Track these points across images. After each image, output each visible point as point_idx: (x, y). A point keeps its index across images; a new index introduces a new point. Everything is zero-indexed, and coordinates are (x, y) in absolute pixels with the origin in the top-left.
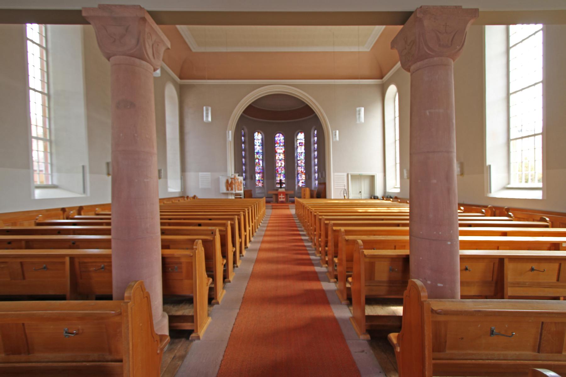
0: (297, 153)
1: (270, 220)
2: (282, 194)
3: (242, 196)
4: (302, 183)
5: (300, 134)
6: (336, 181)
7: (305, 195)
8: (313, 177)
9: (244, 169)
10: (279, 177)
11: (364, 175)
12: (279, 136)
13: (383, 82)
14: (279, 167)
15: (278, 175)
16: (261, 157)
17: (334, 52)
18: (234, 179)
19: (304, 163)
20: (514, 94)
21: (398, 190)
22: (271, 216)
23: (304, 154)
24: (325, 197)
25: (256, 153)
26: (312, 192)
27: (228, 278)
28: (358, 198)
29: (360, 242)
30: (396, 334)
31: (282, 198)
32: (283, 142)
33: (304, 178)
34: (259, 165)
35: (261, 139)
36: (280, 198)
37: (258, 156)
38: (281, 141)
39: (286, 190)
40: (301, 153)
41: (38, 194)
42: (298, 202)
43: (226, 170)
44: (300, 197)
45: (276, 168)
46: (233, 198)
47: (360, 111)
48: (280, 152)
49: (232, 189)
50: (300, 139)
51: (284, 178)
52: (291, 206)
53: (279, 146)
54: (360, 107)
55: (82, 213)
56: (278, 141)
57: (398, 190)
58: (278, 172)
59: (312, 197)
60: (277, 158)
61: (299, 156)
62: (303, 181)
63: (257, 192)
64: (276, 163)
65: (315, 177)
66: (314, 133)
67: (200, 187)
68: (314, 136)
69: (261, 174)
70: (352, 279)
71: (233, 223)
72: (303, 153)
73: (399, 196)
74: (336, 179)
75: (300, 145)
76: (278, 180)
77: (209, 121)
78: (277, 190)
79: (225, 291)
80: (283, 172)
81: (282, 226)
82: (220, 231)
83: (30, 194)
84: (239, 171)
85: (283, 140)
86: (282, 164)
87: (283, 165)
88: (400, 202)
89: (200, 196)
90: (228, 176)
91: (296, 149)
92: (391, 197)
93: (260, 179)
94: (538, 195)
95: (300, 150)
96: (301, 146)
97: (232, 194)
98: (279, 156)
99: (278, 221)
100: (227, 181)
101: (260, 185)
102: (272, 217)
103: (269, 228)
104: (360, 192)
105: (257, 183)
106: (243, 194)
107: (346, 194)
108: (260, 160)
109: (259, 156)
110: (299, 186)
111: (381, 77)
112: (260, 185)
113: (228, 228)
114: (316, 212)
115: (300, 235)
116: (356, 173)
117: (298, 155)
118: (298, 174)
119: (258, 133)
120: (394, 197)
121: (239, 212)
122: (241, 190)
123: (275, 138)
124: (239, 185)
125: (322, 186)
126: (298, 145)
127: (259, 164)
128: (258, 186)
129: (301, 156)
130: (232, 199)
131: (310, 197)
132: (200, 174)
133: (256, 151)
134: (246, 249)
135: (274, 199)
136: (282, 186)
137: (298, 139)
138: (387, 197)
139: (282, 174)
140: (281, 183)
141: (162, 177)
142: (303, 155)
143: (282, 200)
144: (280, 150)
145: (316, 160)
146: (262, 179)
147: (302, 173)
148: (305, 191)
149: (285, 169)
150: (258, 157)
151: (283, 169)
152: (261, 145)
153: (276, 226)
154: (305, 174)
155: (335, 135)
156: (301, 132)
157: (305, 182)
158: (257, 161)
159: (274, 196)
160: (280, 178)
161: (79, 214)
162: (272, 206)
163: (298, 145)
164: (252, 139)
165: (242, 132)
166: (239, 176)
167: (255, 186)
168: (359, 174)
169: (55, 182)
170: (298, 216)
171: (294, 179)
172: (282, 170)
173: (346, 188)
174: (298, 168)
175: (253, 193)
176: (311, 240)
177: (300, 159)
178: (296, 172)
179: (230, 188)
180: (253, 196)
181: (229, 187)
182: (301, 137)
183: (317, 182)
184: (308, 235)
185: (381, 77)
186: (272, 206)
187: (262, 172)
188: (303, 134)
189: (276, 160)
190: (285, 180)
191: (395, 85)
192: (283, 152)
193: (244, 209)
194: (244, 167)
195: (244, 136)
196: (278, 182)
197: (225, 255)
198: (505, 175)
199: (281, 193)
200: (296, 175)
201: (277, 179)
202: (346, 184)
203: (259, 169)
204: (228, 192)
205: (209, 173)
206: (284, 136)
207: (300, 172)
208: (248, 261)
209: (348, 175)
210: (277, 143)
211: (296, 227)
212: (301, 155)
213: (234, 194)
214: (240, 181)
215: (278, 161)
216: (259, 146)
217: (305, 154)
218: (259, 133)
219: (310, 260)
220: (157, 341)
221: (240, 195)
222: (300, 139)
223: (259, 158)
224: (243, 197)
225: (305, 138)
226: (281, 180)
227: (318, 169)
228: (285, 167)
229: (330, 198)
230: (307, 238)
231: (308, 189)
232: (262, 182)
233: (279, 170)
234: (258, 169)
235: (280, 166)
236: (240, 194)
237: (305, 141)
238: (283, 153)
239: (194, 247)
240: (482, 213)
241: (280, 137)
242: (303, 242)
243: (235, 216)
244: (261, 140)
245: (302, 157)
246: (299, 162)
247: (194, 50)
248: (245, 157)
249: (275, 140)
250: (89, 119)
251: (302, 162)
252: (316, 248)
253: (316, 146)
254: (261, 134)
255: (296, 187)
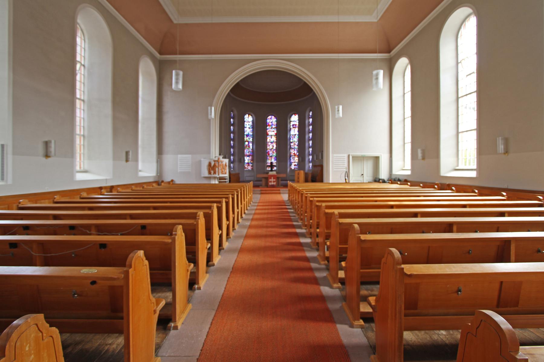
0: (290, 135)
1: (256, 209)
2: (272, 178)
3: (228, 180)
4: (295, 165)
5: (293, 116)
6: (335, 163)
7: (298, 178)
8: (307, 159)
9: (232, 152)
10: (270, 160)
11: (368, 156)
12: (271, 118)
13: (390, 56)
14: (270, 149)
15: (268, 157)
16: (251, 140)
17: (338, 23)
18: (218, 161)
19: (297, 146)
20: (462, 98)
21: (409, 173)
22: (259, 203)
23: (298, 137)
24: (321, 181)
25: (245, 136)
26: (306, 175)
27: (212, 261)
28: (360, 182)
29: (356, 226)
30: (345, 262)
31: (272, 182)
32: (275, 124)
33: (297, 161)
34: (249, 148)
35: (252, 122)
36: (271, 182)
37: (247, 138)
38: (273, 123)
39: (277, 173)
40: (294, 136)
41: (80, 177)
42: (292, 187)
43: (209, 152)
44: (293, 181)
45: (267, 151)
46: (217, 182)
47: (377, 75)
48: (272, 134)
49: (215, 173)
50: (293, 121)
51: (276, 161)
52: (282, 190)
53: (271, 129)
54: (377, 69)
55: (113, 191)
56: (270, 124)
57: (409, 173)
58: (269, 154)
59: (306, 181)
60: (268, 140)
61: (292, 138)
62: (296, 164)
63: (245, 175)
64: (268, 145)
65: (309, 159)
66: (309, 115)
67: (179, 171)
68: (309, 118)
69: (251, 157)
70: (346, 263)
71: (227, 201)
72: (296, 135)
73: (409, 179)
74: (335, 161)
75: (293, 127)
76: (269, 163)
77: (180, 89)
78: (268, 173)
79: (220, 257)
80: (274, 154)
81: (271, 219)
82: (204, 213)
83: (72, 176)
84: (224, 152)
85: (276, 123)
86: (273, 146)
87: (275, 148)
88: (423, 187)
89: (178, 181)
90: (211, 158)
91: (289, 131)
92: (399, 180)
93: (249, 162)
94: (473, 174)
95: (294, 132)
96: (294, 128)
97: (215, 178)
98: (271, 139)
99: (266, 211)
100: (210, 164)
101: (249, 168)
102: (260, 204)
103: (256, 216)
104: (362, 175)
105: (246, 166)
106: (228, 178)
107: (347, 177)
108: (250, 143)
109: (249, 139)
110: (291, 169)
111: (389, 51)
112: (250, 168)
113: (214, 210)
114: (307, 194)
115: (297, 235)
116: (359, 154)
117: (291, 137)
118: (291, 156)
119: (249, 115)
120: (403, 180)
121: (228, 194)
122: (226, 173)
123: (267, 120)
124: (224, 168)
125: (319, 169)
126: (292, 127)
127: (249, 147)
128: (247, 169)
129: (294, 138)
130: (215, 184)
131: (322, 183)
132: (179, 156)
133: (245, 134)
134: (242, 218)
135: (263, 182)
136: (273, 169)
137: (292, 121)
138: (393, 180)
139: (274, 157)
140: (272, 166)
141: (130, 159)
142: (297, 137)
143: (272, 183)
144: (272, 132)
145: (311, 142)
146: (252, 162)
147: (295, 155)
148: (298, 174)
149: (276, 151)
150: (248, 140)
151: (274, 151)
152: (251, 127)
153: (263, 219)
154: (298, 156)
155: (338, 111)
156: (295, 114)
157: (297, 164)
158: (247, 143)
159: (264, 180)
160: (271, 161)
161: (111, 192)
162: (261, 191)
163: (292, 127)
164: (242, 122)
165: (231, 114)
166: (223, 158)
167: (244, 170)
168: (362, 155)
169: (86, 168)
170: (292, 204)
171: (286, 162)
172: (273, 153)
173: (347, 171)
174: (291, 150)
175: (240, 176)
176: (317, 246)
177: (293, 141)
178: (288, 154)
179: (212, 172)
180: (241, 180)
181: (212, 170)
182: (295, 119)
183: (311, 164)
184: (310, 235)
185: (389, 51)
186: (261, 191)
187: (252, 155)
188: (297, 116)
189: (267, 142)
190: (276, 163)
191: (407, 58)
192: (275, 134)
193: (237, 190)
194: (232, 150)
195: (233, 118)
196: (269, 164)
197: (209, 237)
198: (455, 159)
199: (272, 176)
200: (288, 158)
201: (267, 162)
202: (346, 165)
203: (249, 151)
204: (210, 176)
205: (190, 156)
206: (276, 119)
207: (293, 154)
208: (243, 227)
209: (349, 156)
210: (269, 125)
211: (291, 220)
212: (294, 137)
213: (217, 178)
214: (224, 163)
215: (269, 144)
216: (249, 128)
217: (298, 136)
218: (250, 116)
219: (291, 219)
220: (153, 303)
221: (225, 179)
222: (293, 121)
223: (249, 141)
224: (228, 181)
225: (299, 120)
226: (272, 163)
227: (312, 151)
228: (276, 149)
229: (327, 182)
230: (308, 240)
231: (302, 172)
232: (252, 165)
233: (270, 152)
234: (248, 152)
235: (272, 149)
236: (225, 178)
237: (299, 122)
238: (275, 136)
239: (174, 233)
240: (421, 186)
241: (272, 119)
242: (303, 251)
243: (212, 204)
244: (251, 122)
245: (296, 139)
246: (292, 144)
247: (175, 22)
248: (233, 140)
249: (267, 122)
250: (115, 118)
251: (295, 144)
252: (299, 217)
253: (311, 127)
254: (251, 116)
255: (288, 170)
